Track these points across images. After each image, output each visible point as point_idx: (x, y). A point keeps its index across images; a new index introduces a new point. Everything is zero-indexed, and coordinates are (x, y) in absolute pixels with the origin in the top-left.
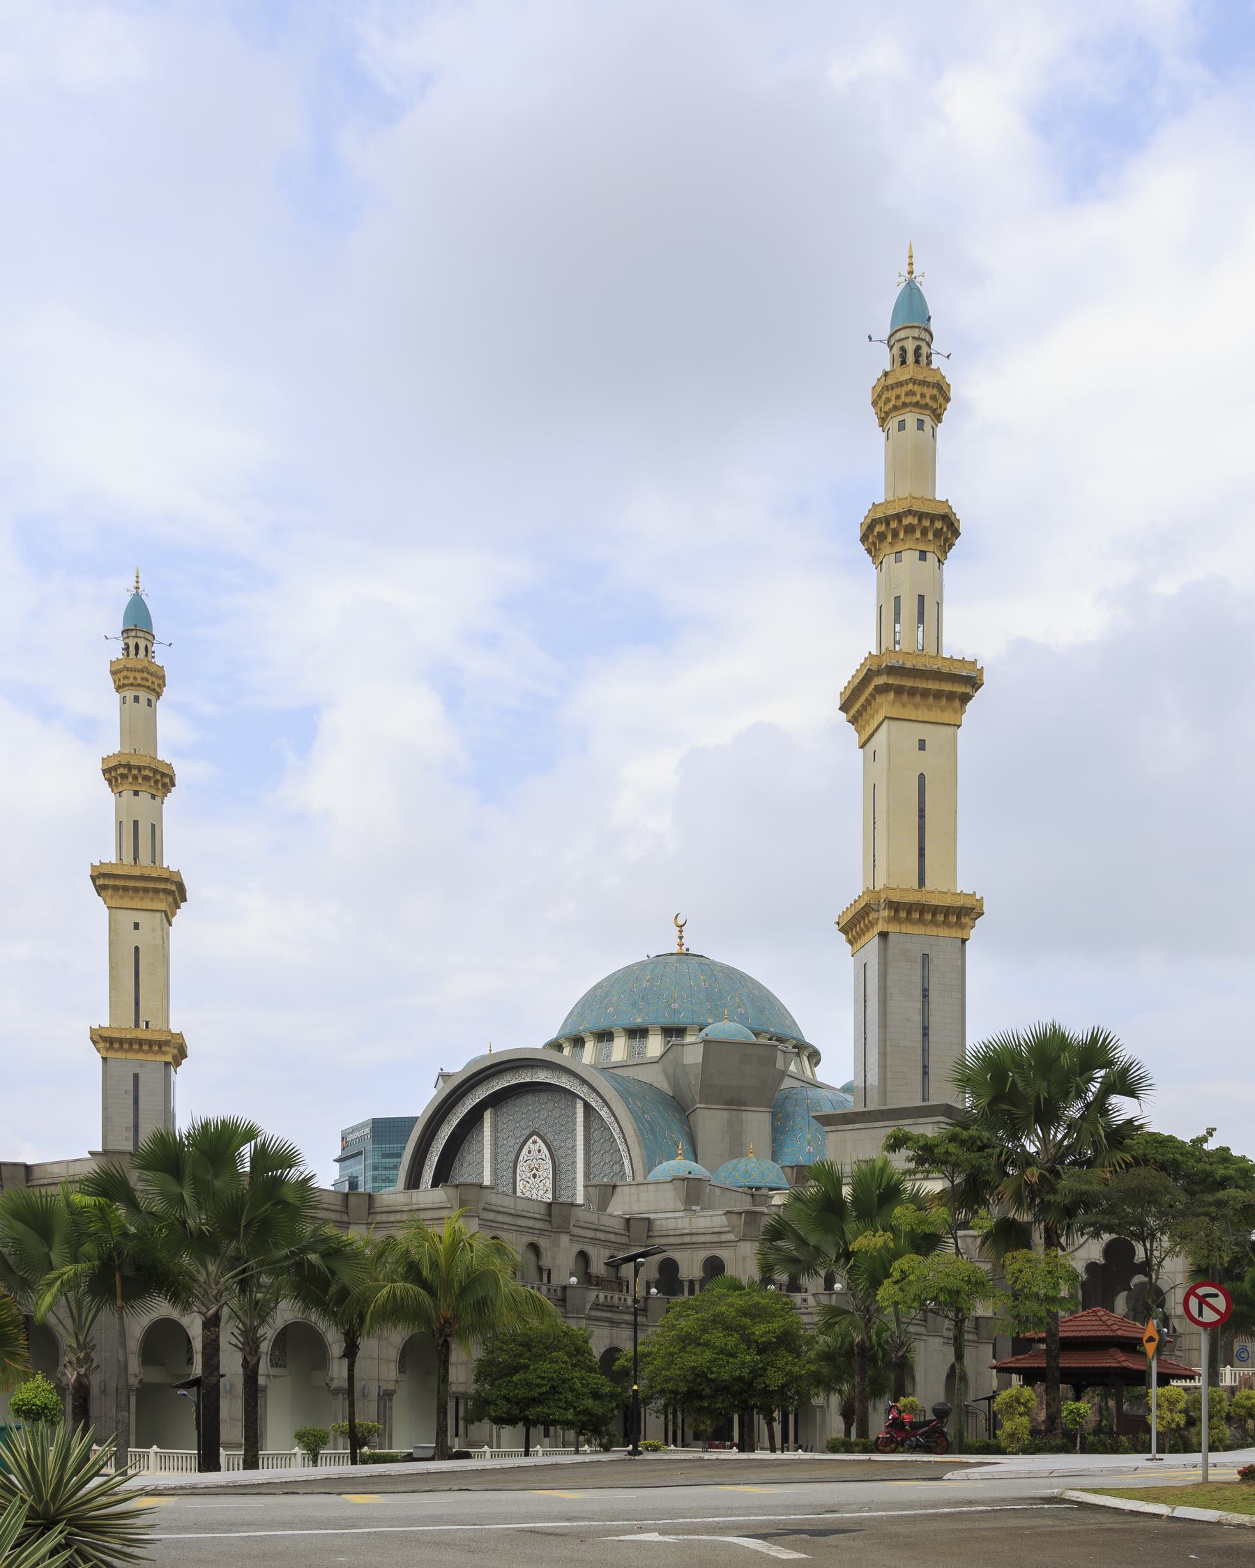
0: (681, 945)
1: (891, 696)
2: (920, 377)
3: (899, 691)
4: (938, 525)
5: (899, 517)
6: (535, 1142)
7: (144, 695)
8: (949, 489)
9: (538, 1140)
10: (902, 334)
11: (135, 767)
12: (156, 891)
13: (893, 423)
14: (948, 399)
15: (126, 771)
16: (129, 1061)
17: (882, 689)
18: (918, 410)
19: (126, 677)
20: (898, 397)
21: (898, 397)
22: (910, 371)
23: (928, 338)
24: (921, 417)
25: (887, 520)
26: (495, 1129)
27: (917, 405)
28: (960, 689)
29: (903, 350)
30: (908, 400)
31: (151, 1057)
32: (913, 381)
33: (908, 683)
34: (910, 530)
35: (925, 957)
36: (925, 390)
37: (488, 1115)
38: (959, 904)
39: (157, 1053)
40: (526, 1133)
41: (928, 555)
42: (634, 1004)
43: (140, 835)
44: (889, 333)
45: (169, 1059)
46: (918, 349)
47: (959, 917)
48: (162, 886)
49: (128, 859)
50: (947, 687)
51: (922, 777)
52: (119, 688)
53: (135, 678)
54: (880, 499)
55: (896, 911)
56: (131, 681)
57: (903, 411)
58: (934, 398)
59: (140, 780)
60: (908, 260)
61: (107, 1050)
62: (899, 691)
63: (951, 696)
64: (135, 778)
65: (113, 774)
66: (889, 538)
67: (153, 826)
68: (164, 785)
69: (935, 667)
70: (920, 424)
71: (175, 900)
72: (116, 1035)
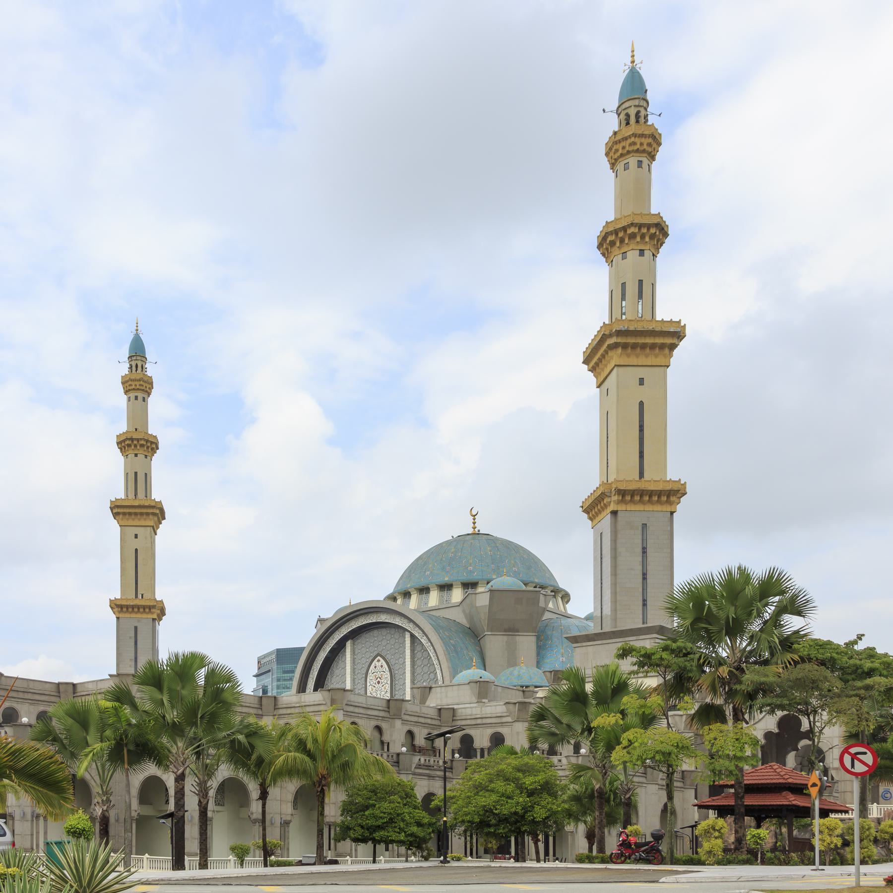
0: (474, 528)
1: (620, 350)
2: (640, 132)
3: (625, 346)
4: (653, 231)
5: (624, 229)
6: (379, 661)
7: (140, 395)
8: (659, 205)
12: (148, 514)
13: (620, 166)
14: (659, 144)
15: (637, 230)
16: (132, 619)
17: (615, 346)
21: (624, 148)
22: (633, 128)
23: (645, 104)
24: (640, 159)
25: (616, 232)
26: (353, 653)
27: (637, 151)
28: (668, 341)
29: (628, 115)
30: (631, 148)
31: (145, 616)
32: (634, 135)
33: (631, 340)
34: (632, 236)
35: (644, 526)
36: (643, 140)
37: (349, 644)
38: (668, 488)
42: (443, 569)
43: (138, 480)
44: (617, 105)
45: (155, 616)
46: (638, 113)
47: (668, 497)
48: (150, 511)
49: (131, 495)
50: (145, 511)
52: (126, 392)
54: (611, 218)
55: (623, 496)
58: (649, 145)
59: (647, 239)
60: (630, 54)
62: (625, 346)
63: (662, 347)
64: (148, 448)
65: (644, 230)
66: (638, 239)
68: (152, 449)
69: (651, 328)
70: (640, 164)
72: (124, 603)
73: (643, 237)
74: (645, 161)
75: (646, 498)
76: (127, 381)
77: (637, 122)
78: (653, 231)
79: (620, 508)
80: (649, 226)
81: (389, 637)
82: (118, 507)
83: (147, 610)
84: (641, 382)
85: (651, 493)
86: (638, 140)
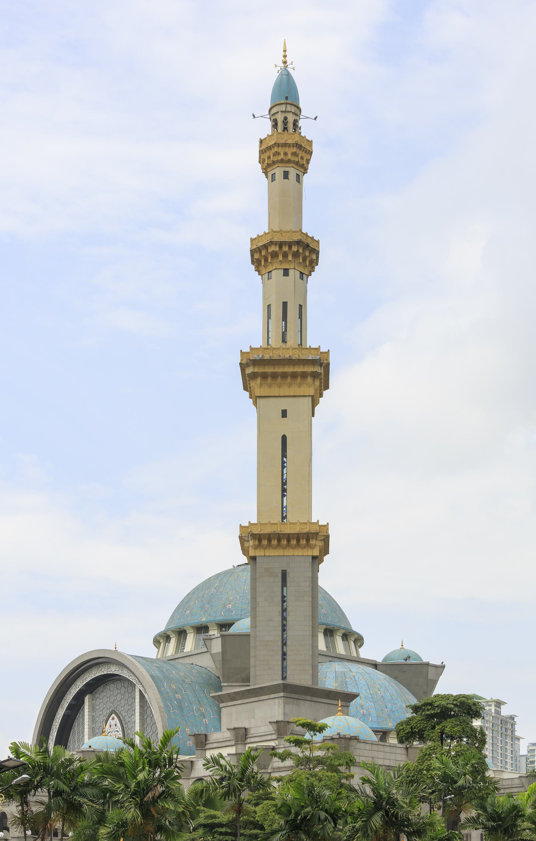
1: (259, 381)
2: (283, 141)
3: (264, 376)
4: (295, 249)
6: (113, 719)
8: (310, 227)
9: (115, 717)
10: (274, 110)
11: (285, 243)
12: (304, 375)
14: (310, 153)
15: (277, 249)
16: (275, 557)
18: (284, 165)
19: (277, 154)
20: (269, 158)
21: (269, 158)
23: (293, 109)
24: (286, 169)
25: (281, 244)
26: (93, 709)
27: (282, 161)
30: (275, 159)
31: (299, 552)
33: (269, 370)
34: (274, 255)
35: (284, 574)
36: (287, 150)
37: (87, 699)
38: (306, 531)
39: (304, 547)
40: (106, 712)
41: (291, 272)
43: (288, 314)
44: (269, 106)
45: (316, 552)
47: (308, 540)
48: (309, 369)
49: (275, 341)
50: (299, 369)
51: (284, 439)
53: (286, 154)
55: (260, 541)
56: (282, 156)
57: (274, 167)
58: (295, 154)
59: (290, 258)
60: (283, 53)
61: (256, 548)
62: (264, 376)
65: (285, 249)
66: (280, 258)
67: (301, 306)
69: (287, 356)
70: (286, 175)
71: (320, 386)
72: (268, 530)
73: (285, 255)
74: (293, 172)
75: (284, 542)
76: (269, 148)
77: (285, 129)
78: (295, 249)
79: (259, 553)
80: (290, 245)
81: (116, 692)
82: (255, 362)
83: (303, 542)
84: (284, 414)
85: (289, 537)
86: (281, 150)
